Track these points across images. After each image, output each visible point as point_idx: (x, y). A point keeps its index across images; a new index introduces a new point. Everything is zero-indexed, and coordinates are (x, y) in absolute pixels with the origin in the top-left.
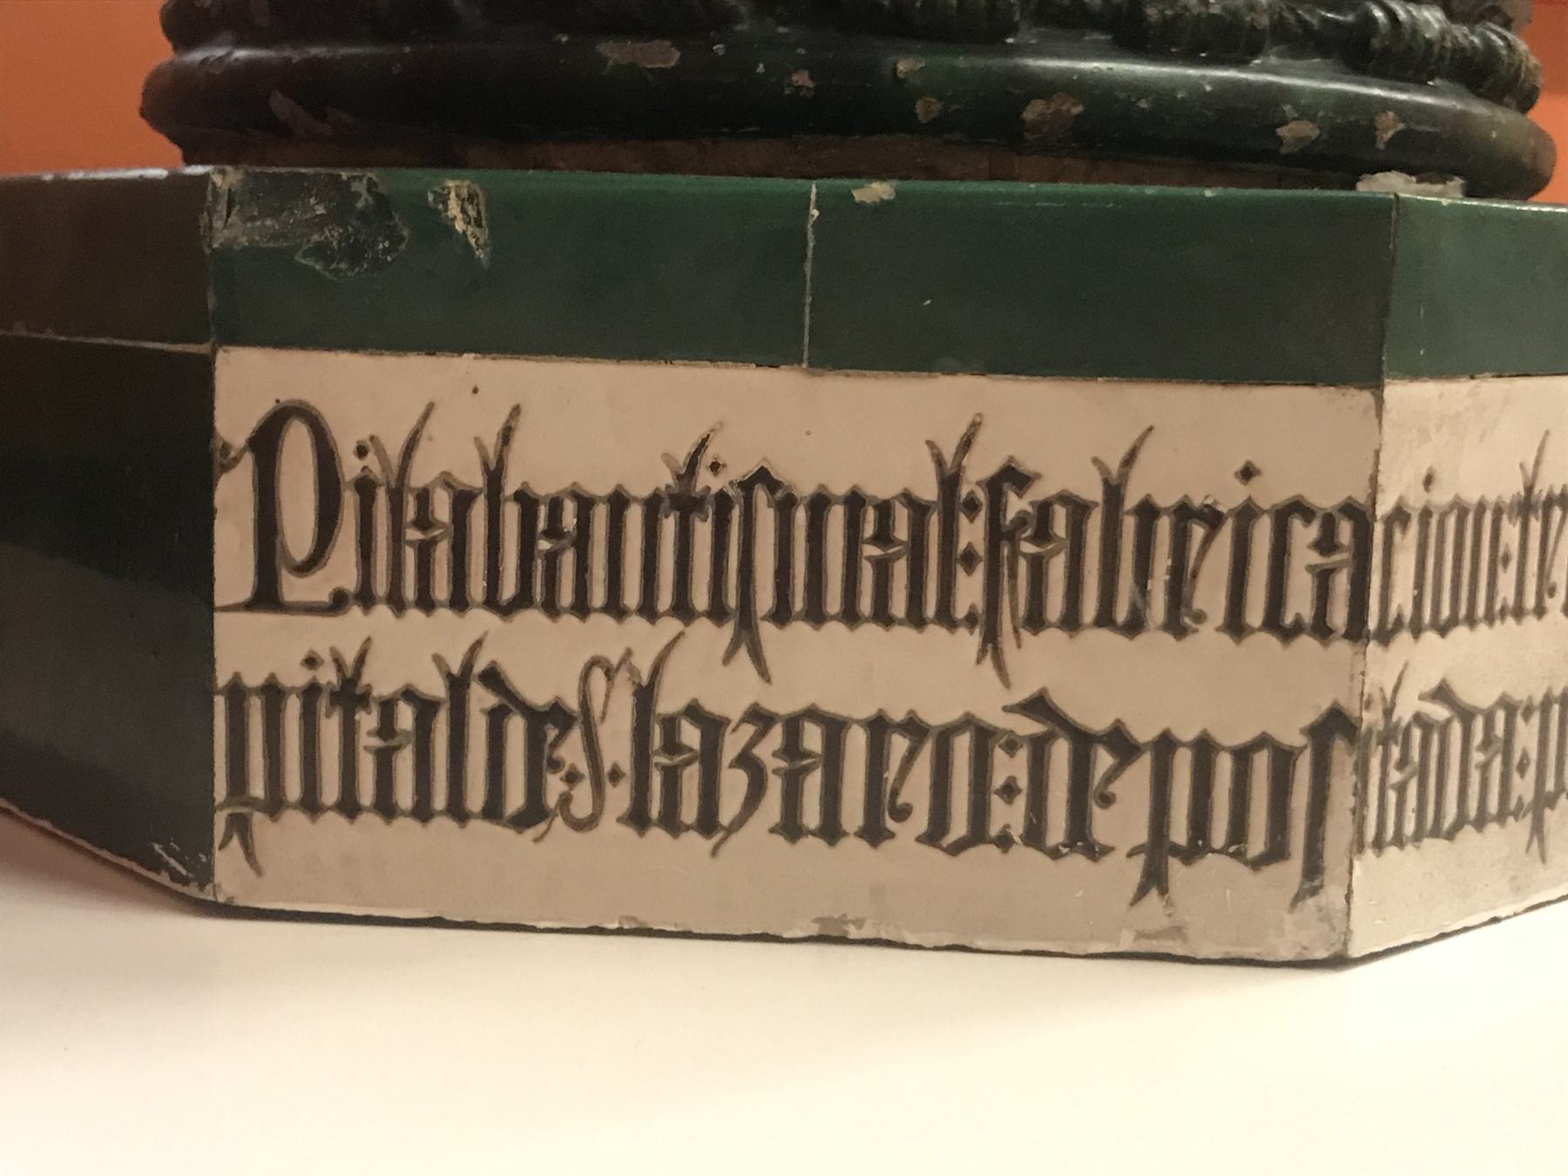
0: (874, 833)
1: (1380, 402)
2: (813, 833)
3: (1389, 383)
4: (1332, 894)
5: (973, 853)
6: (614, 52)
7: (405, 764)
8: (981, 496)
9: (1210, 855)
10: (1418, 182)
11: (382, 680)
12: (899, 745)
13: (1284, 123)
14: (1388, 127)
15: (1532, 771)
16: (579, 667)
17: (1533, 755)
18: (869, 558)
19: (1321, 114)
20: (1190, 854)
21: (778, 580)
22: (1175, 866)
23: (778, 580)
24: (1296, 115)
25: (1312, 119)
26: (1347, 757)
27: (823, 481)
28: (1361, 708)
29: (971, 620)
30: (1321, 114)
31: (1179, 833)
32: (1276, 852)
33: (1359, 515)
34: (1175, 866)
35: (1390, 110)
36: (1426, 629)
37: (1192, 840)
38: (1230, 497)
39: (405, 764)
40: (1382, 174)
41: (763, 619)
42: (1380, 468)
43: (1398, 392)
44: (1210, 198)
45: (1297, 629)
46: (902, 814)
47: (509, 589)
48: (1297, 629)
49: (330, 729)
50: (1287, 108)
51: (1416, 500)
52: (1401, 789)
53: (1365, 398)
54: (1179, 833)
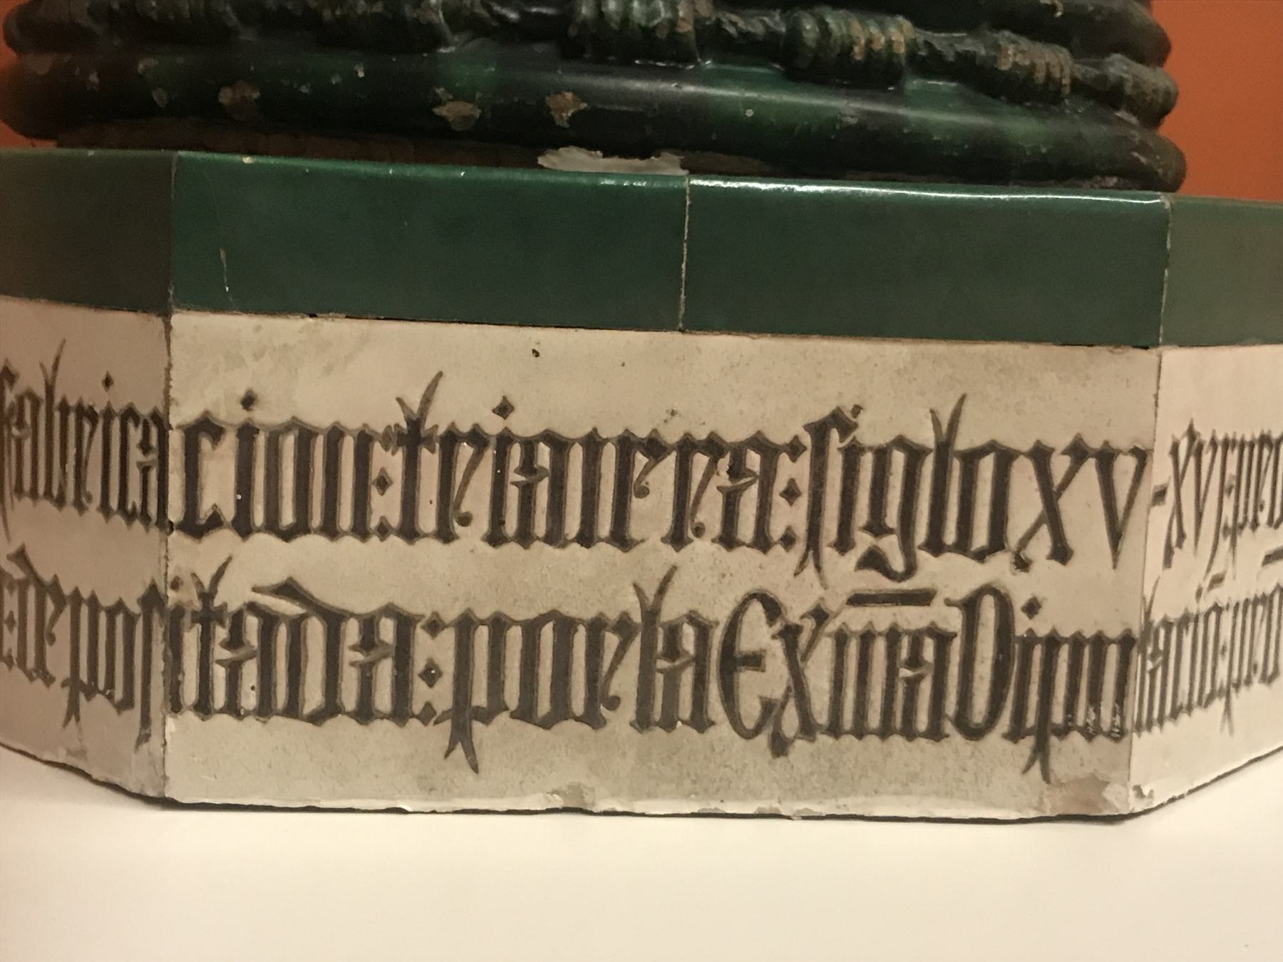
0: (592, 719)
1: (168, 328)
2: (349, 714)
3: (177, 312)
4: (155, 741)
5: (330, 723)
6: (664, 65)
7: (250, 672)
8: (807, 440)
9: (411, 720)
10: (604, 156)
11: (232, 595)
12: (611, 641)
13: (439, 103)
14: (565, 107)
15: (1227, 654)
16: (740, 593)
17: (1228, 647)
18: (515, 483)
19: (478, 95)
20: (486, 716)
21: (239, 497)
22: (1054, 740)
23: (239, 497)
24: (451, 97)
25: (470, 100)
26: (159, 628)
27: (477, 420)
28: (166, 588)
29: (788, 540)
30: (478, 95)
31: (480, 698)
32: (126, 704)
33: (160, 421)
34: (1054, 740)
35: (568, 91)
36: (114, 513)
37: (1067, 720)
38: (493, 426)
39: (250, 672)
40: (566, 149)
41: (920, 548)
42: (172, 383)
43: (184, 321)
44: (248, 164)
45: (215, 521)
46: (614, 703)
47: (288, 517)
48: (215, 521)
49: (191, 639)
50: (440, 91)
51: (230, 414)
52: (1153, 673)
53: (157, 323)
54: (480, 698)
